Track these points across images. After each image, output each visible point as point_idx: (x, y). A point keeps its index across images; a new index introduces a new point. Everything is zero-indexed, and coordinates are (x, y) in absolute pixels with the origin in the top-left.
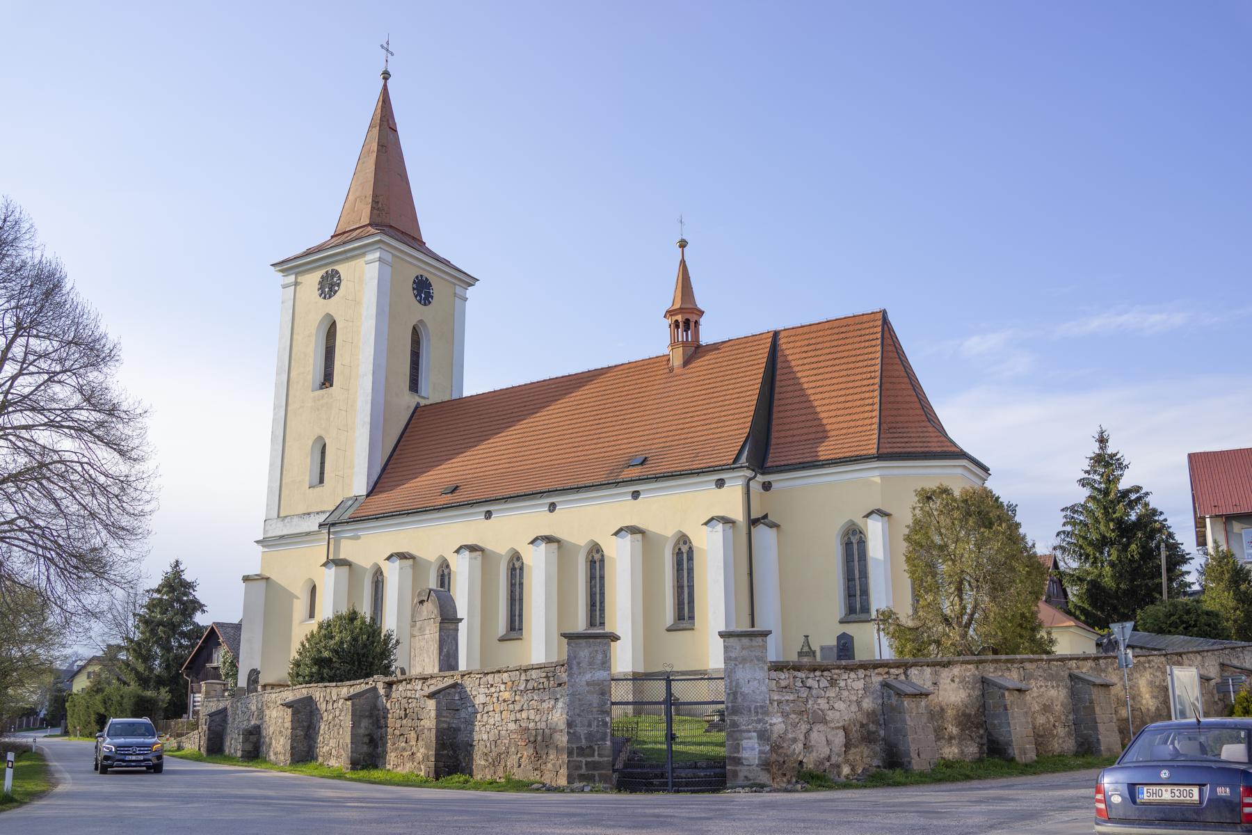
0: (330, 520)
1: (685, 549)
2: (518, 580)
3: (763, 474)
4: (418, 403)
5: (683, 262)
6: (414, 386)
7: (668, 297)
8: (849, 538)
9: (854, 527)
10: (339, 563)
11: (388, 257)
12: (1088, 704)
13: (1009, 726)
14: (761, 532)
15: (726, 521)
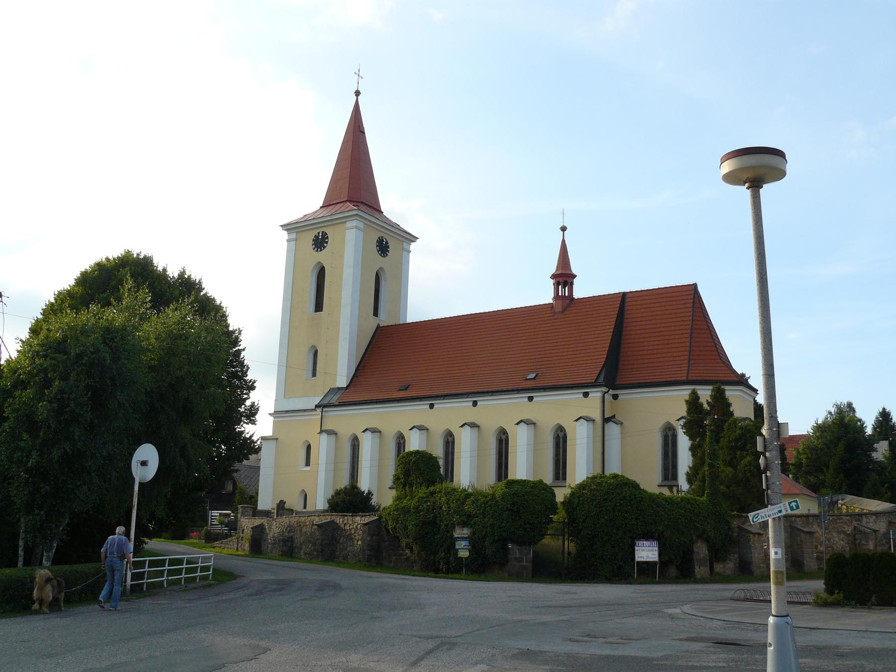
0: (325, 402)
1: (561, 435)
2: (450, 450)
3: (613, 389)
4: (379, 324)
5: (563, 242)
6: (376, 313)
7: (552, 267)
8: (667, 432)
9: (670, 426)
10: (330, 432)
11: (361, 225)
12: (799, 543)
13: (751, 554)
14: (612, 428)
15: (588, 419)
